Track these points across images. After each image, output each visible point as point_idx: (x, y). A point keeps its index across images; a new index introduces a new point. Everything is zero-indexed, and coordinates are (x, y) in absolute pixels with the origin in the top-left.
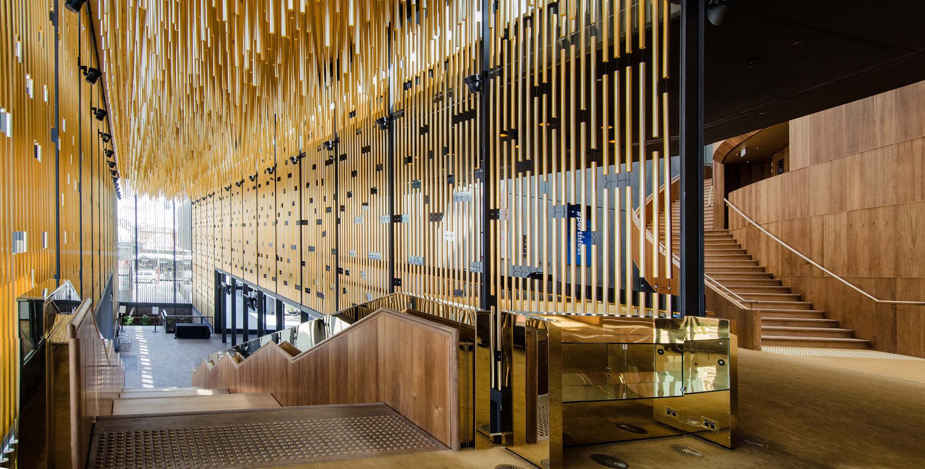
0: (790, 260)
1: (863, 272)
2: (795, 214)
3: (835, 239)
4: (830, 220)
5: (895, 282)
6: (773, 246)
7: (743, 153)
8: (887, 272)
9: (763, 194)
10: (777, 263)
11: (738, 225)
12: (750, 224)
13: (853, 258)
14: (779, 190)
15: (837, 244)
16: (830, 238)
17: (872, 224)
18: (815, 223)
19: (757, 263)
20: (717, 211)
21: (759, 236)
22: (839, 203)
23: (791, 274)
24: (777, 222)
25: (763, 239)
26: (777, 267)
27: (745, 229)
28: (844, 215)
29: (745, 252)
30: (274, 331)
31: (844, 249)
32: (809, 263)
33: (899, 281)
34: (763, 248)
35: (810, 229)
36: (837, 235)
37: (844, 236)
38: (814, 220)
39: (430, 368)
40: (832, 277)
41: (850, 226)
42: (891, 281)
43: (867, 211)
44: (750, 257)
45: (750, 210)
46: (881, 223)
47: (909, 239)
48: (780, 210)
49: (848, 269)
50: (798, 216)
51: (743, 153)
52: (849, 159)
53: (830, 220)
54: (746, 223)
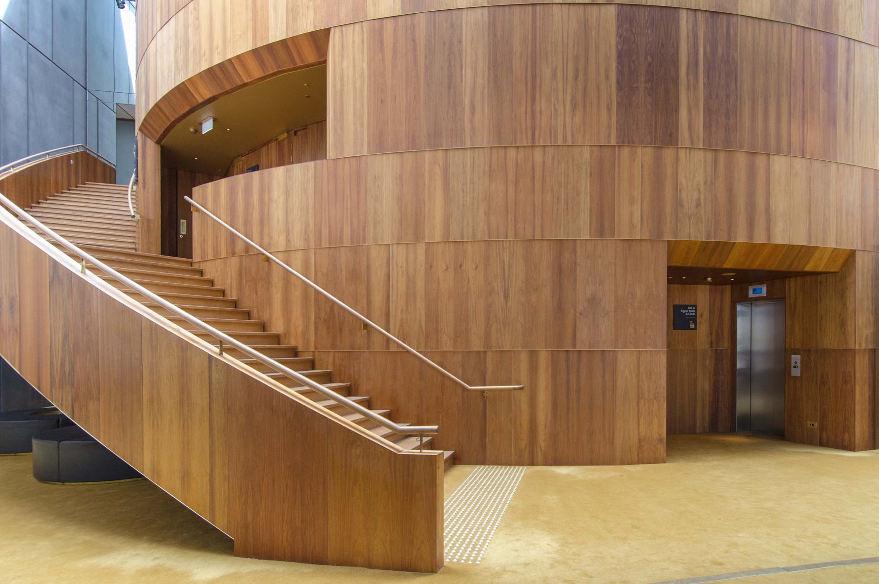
0: (331, 320)
1: (447, 345)
2: (341, 237)
3: (408, 288)
4: (399, 253)
5: (485, 358)
6: (296, 294)
7: (208, 127)
8: (476, 345)
9: (277, 194)
10: (307, 327)
11: (216, 252)
12: (248, 247)
13: (433, 318)
14: (311, 191)
15: (410, 296)
16: (399, 286)
17: (459, 267)
18: (377, 257)
19: (263, 327)
20: (149, 230)
21: (269, 275)
22: (412, 226)
23: (334, 346)
24: (306, 250)
25: (277, 279)
26: (305, 333)
27: (234, 261)
28: (421, 249)
29: (235, 303)
30: (368, 347)
31: (421, 305)
32: (366, 326)
33: (489, 356)
34: (277, 297)
35: (368, 266)
36: (411, 281)
37: (420, 284)
38: (374, 252)
39: (649, 85)
40: (408, 352)
41: (429, 267)
42: (481, 355)
43: (452, 245)
44: (248, 315)
45: (247, 223)
46: (469, 266)
47: (501, 294)
48: (312, 224)
49: (427, 337)
50: (347, 242)
51: (208, 127)
52: (428, 155)
53: (399, 253)
54: (239, 247)
